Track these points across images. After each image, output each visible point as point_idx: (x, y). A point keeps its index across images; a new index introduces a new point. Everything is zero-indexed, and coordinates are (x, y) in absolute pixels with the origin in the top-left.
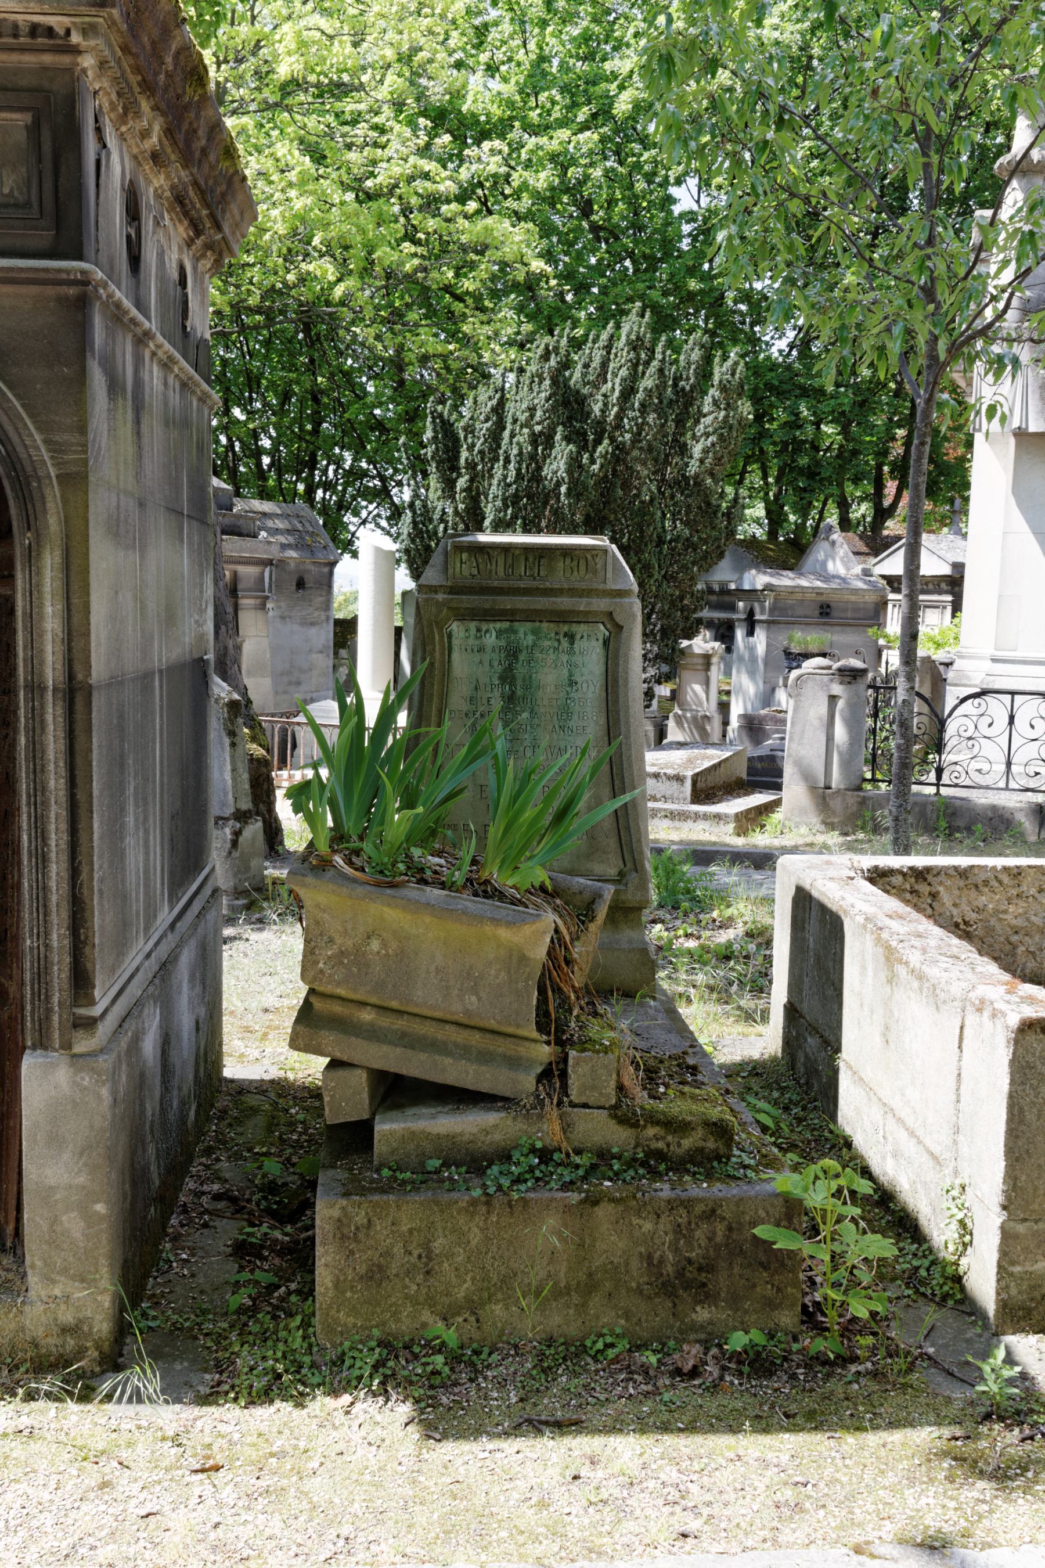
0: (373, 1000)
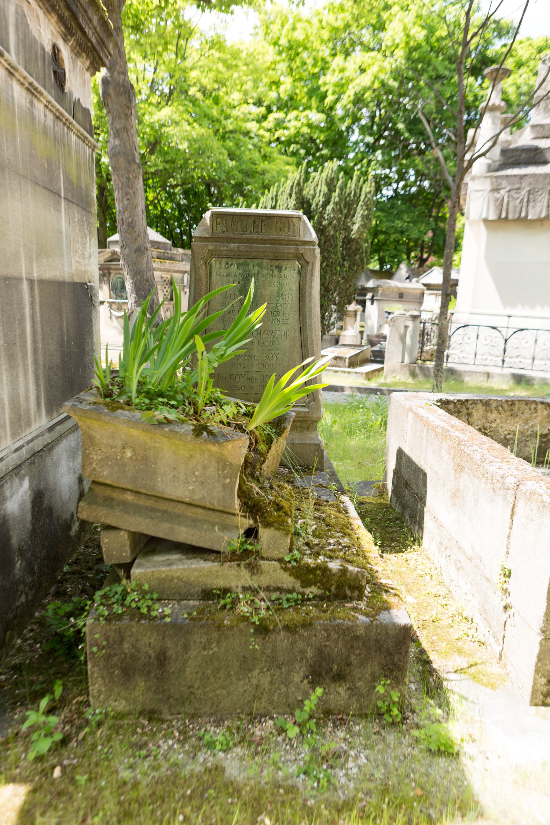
0: (130, 487)
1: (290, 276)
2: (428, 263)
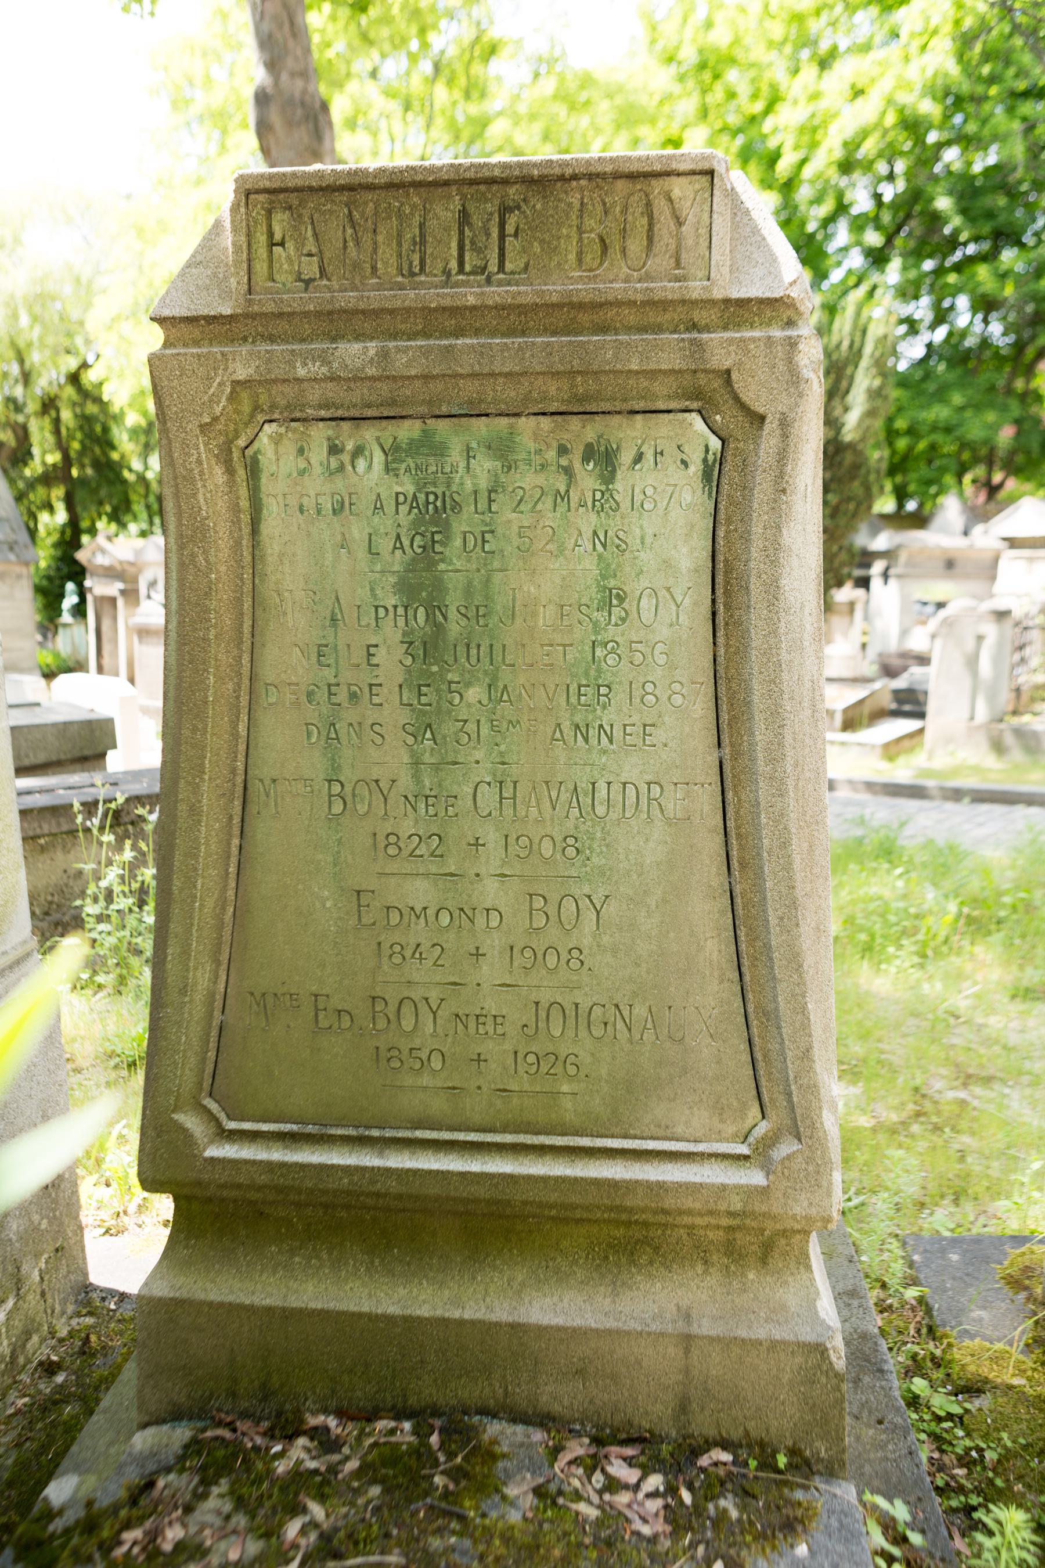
1: (662, 499)
2: (1002, 495)
